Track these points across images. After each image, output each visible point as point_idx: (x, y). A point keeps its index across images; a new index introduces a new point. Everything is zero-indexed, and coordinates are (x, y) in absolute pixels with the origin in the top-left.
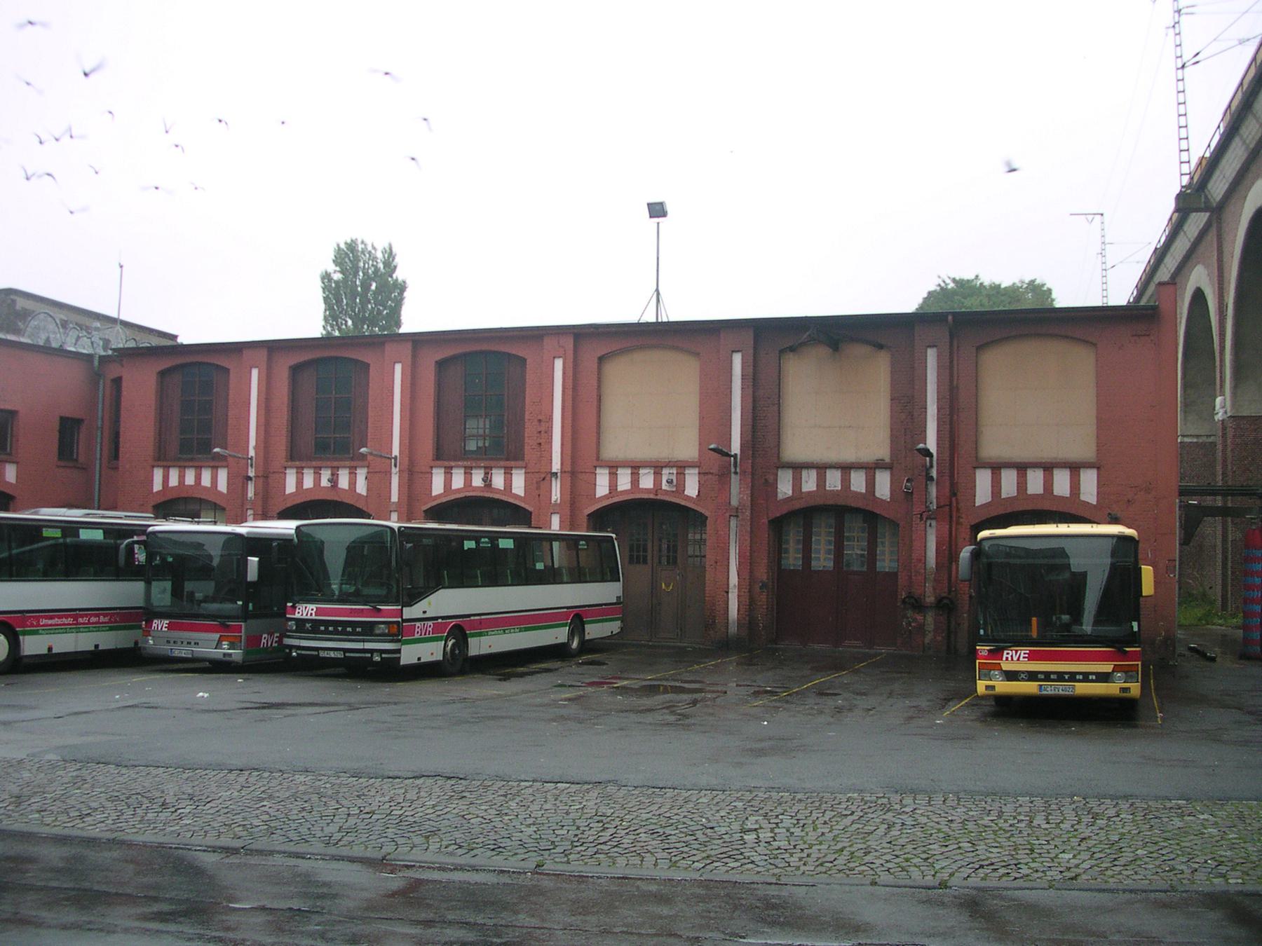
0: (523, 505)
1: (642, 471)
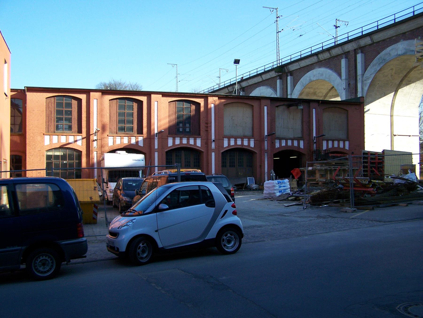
0: (201, 149)
1: (231, 139)
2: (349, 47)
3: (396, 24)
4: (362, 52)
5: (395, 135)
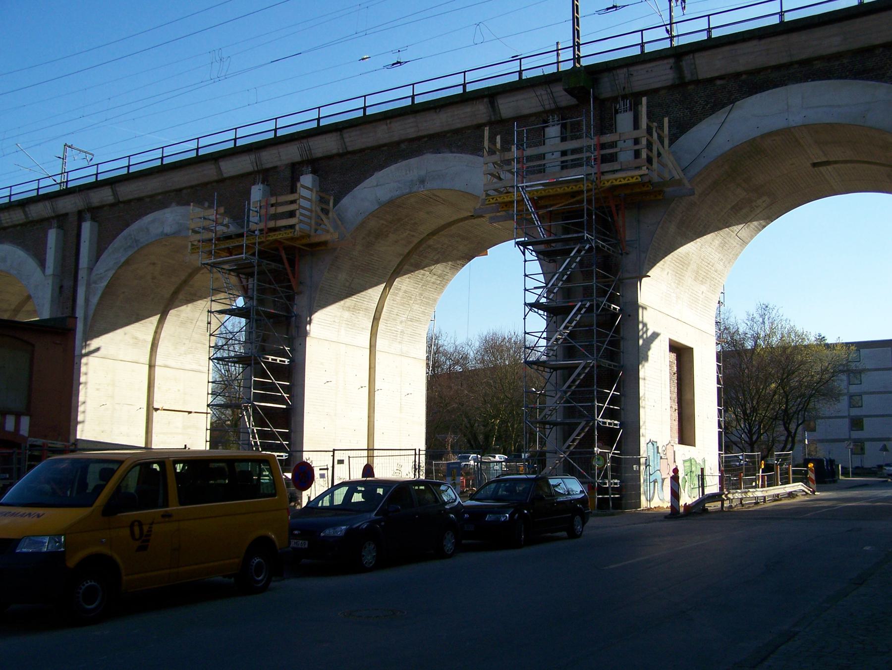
2: (67, 205)
3: (164, 169)
4: (93, 219)
5: (157, 410)
